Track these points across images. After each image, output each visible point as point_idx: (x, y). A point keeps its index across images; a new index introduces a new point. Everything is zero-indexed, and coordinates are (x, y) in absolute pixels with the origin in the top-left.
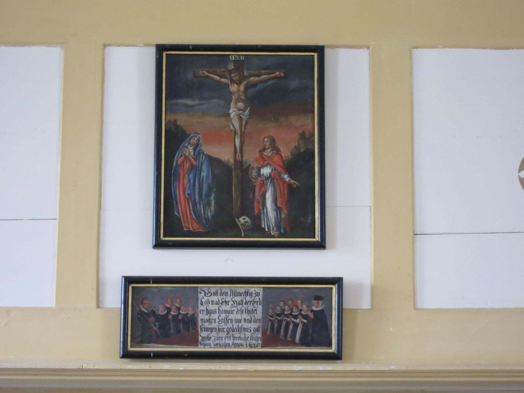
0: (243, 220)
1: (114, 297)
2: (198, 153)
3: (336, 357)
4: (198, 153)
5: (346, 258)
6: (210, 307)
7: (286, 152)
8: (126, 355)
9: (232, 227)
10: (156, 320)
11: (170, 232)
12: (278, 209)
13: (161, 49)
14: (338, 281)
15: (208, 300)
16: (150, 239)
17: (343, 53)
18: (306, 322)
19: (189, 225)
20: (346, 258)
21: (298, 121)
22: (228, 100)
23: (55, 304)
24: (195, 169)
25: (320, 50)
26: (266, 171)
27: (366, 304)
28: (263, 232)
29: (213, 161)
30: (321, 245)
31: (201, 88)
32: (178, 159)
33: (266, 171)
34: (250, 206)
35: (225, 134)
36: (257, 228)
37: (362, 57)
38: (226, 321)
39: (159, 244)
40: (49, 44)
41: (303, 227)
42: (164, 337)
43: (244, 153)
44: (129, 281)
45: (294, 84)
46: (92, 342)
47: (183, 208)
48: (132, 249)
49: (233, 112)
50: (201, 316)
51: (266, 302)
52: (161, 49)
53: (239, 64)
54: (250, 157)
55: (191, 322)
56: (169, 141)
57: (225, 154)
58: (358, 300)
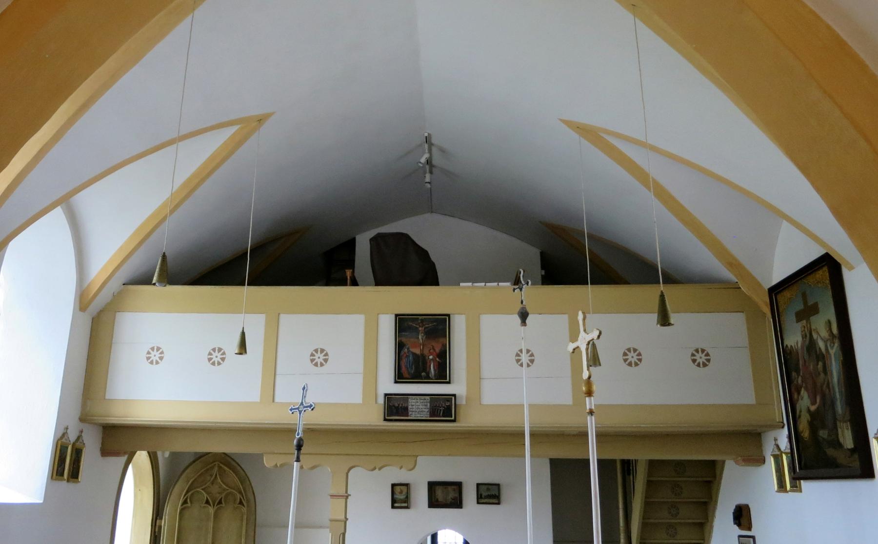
0: (423, 374)
1: (381, 400)
2: (409, 351)
3: (454, 421)
4: (409, 351)
5: (457, 387)
6: (412, 403)
7: (438, 350)
8: (385, 420)
9: (420, 377)
10: (395, 408)
11: (400, 377)
12: (435, 370)
13: (396, 315)
14: (454, 395)
15: (412, 402)
16: (393, 380)
17: (456, 316)
18: (443, 409)
19: (406, 375)
20: (457, 387)
21: (441, 340)
22: (418, 332)
23: (820, 272)
24: (407, 357)
25: (449, 315)
26: (431, 357)
27: (464, 402)
28: (429, 378)
29: (414, 354)
30: (449, 383)
31: (410, 328)
32: (402, 353)
33: (431, 357)
34: (425, 369)
35: (417, 345)
36: (428, 377)
37: (463, 317)
38: (418, 408)
39: (396, 382)
40: (360, 313)
41: (443, 376)
42: (398, 414)
43: (277, 377)
44: (386, 395)
45: (441, 327)
46: (374, 417)
47: (403, 369)
48: (387, 384)
49: (420, 337)
50: (410, 407)
51: (430, 402)
52: (396, 315)
53: (422, 321)
54: (426, 352)
55: (406, 409)
56: (400, 346)
57: (417, 351)
58: (461, 401)
